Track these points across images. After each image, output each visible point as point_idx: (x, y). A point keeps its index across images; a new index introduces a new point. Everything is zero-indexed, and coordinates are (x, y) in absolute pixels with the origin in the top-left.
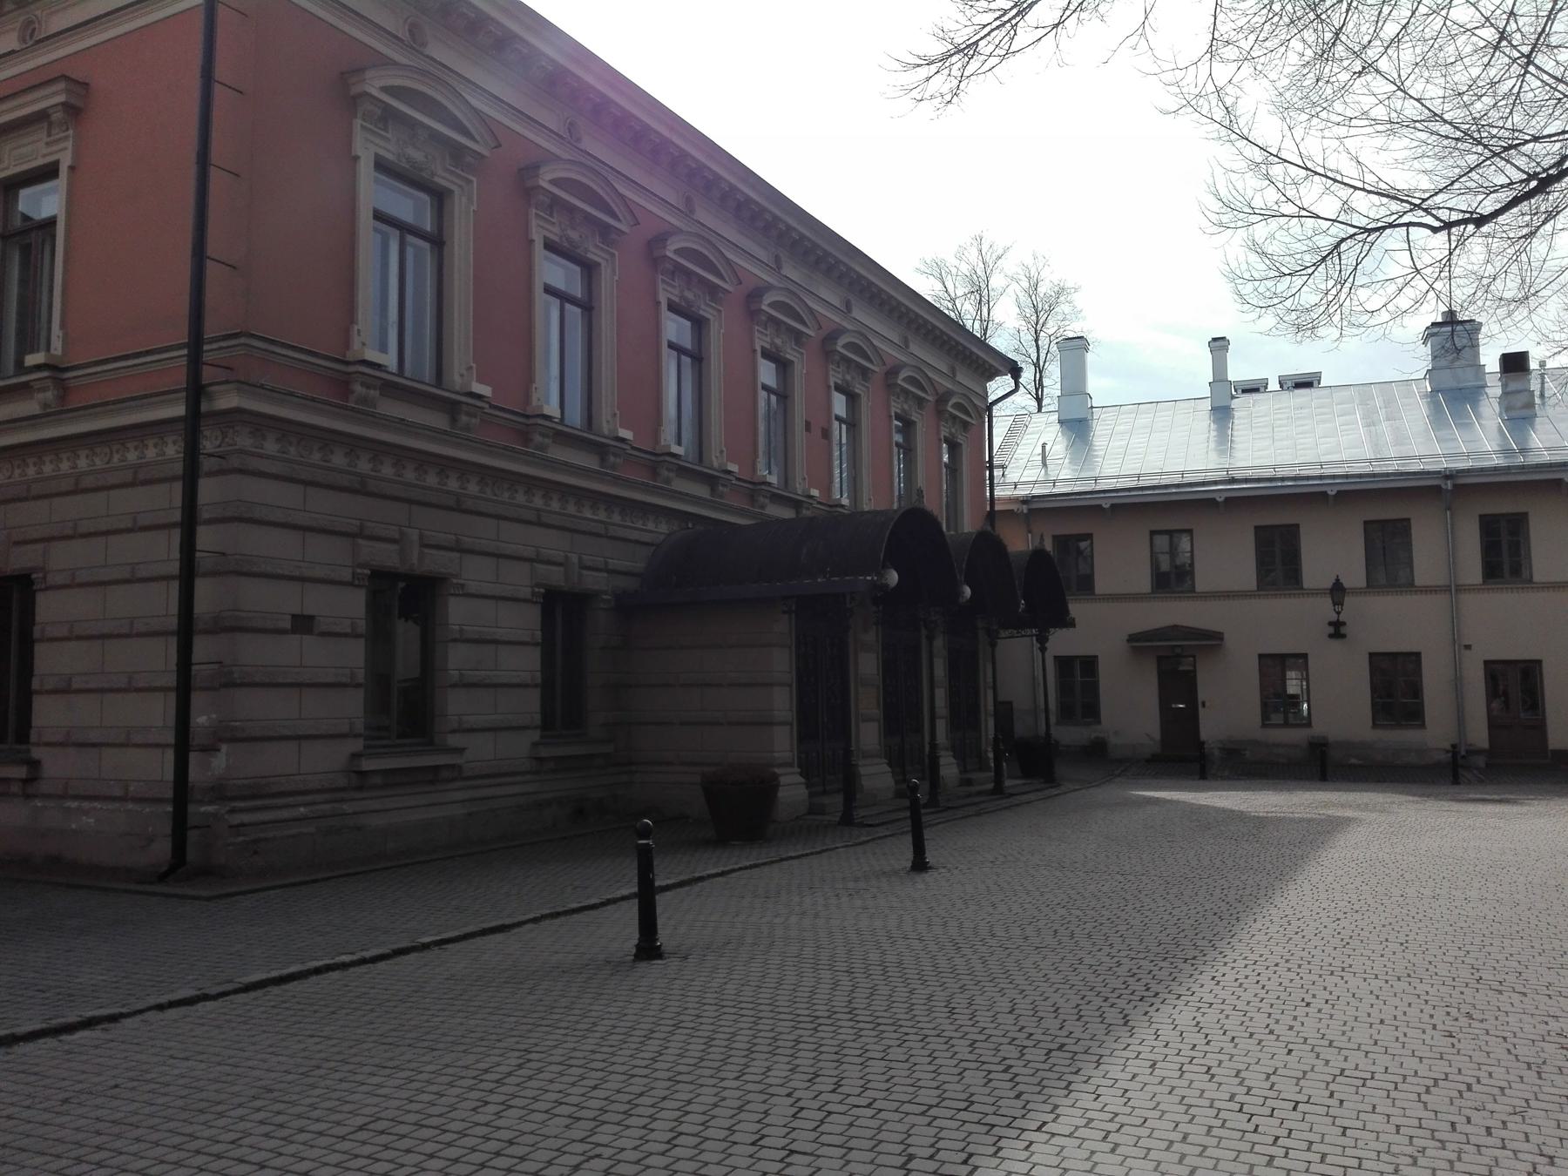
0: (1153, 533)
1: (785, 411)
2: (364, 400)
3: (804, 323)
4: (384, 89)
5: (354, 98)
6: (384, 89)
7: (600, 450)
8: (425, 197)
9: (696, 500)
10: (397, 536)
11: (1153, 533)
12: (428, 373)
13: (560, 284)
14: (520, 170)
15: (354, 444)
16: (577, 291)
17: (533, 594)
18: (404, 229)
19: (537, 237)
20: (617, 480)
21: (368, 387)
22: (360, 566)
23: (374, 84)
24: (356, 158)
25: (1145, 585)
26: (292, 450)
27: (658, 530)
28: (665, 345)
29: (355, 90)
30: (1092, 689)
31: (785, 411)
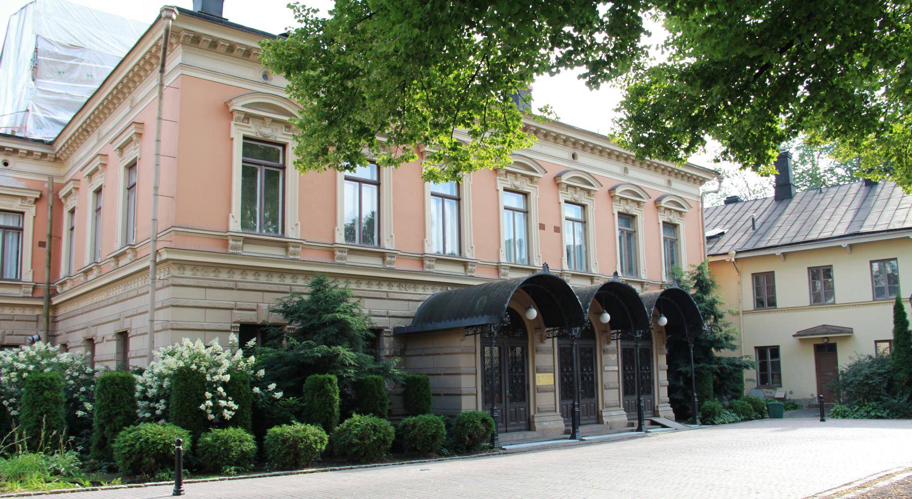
0: (871, 262)
1: (527, 220)
2: (235, 248)
3: (641, 197)
4: (244, 106)
5: (231, 113)
6: (244, 106)
7: (465, 264)
8: (579, 207)
9: (460, 277)
10: (255, 308)
11: (871, 262)
12: (456, 252)
13: (572, 216)
14: (555, 178)
15: (231, 268)
16: (521, 206)
17: (232, 327)
18: (443, 197)
19: (562, 201)
20: (294, 261)
21: (236, 241)
22: (235, 322)
23: (237, 105)
24: (232, 139)
25: (869, 295)
26: (199, 273)
27: (428, 293)
28: (501, 208)
29: (231, 109)
30: (777, 366)
31: (527, 220)
